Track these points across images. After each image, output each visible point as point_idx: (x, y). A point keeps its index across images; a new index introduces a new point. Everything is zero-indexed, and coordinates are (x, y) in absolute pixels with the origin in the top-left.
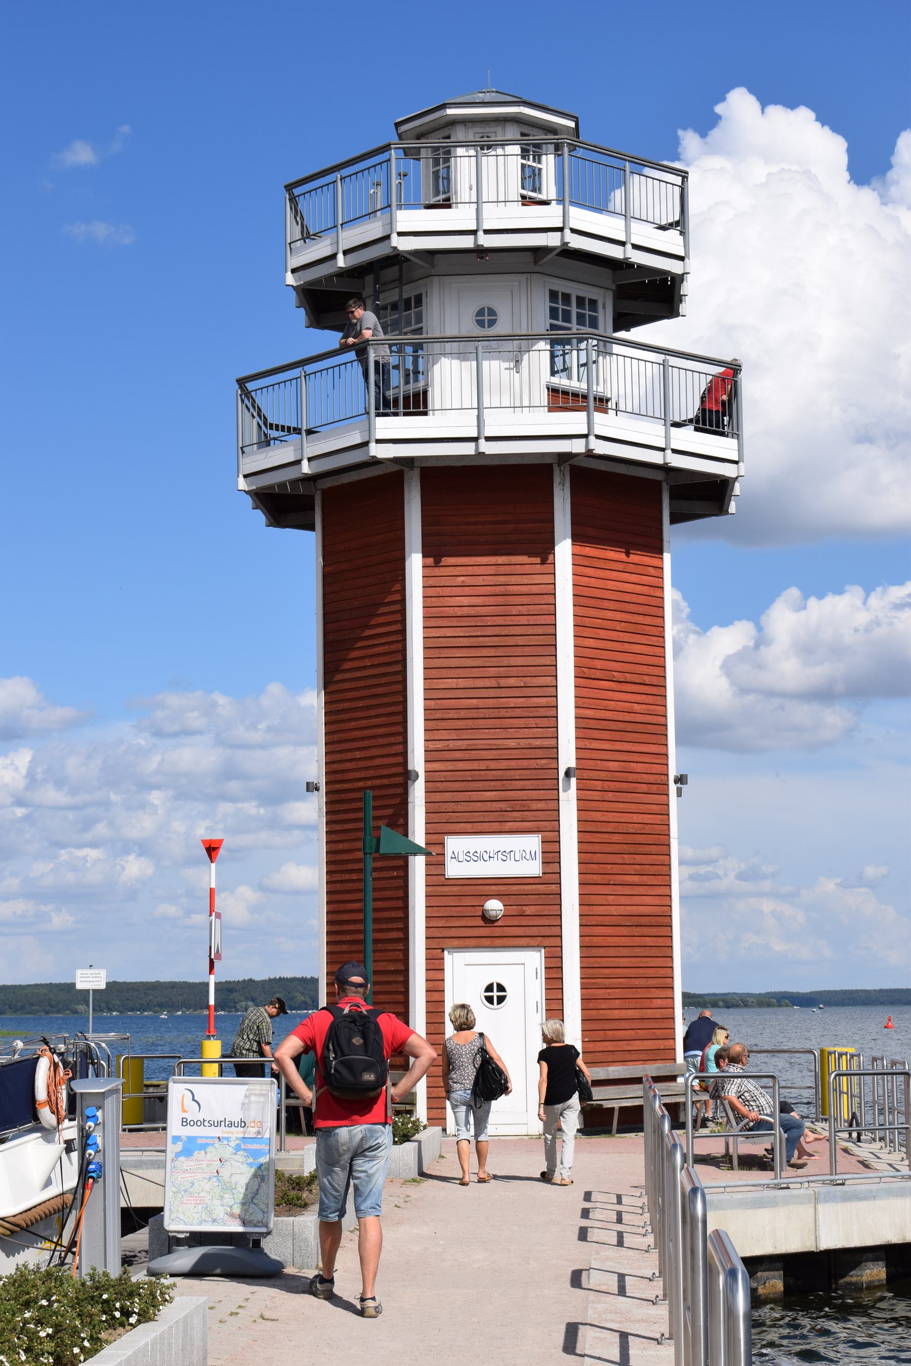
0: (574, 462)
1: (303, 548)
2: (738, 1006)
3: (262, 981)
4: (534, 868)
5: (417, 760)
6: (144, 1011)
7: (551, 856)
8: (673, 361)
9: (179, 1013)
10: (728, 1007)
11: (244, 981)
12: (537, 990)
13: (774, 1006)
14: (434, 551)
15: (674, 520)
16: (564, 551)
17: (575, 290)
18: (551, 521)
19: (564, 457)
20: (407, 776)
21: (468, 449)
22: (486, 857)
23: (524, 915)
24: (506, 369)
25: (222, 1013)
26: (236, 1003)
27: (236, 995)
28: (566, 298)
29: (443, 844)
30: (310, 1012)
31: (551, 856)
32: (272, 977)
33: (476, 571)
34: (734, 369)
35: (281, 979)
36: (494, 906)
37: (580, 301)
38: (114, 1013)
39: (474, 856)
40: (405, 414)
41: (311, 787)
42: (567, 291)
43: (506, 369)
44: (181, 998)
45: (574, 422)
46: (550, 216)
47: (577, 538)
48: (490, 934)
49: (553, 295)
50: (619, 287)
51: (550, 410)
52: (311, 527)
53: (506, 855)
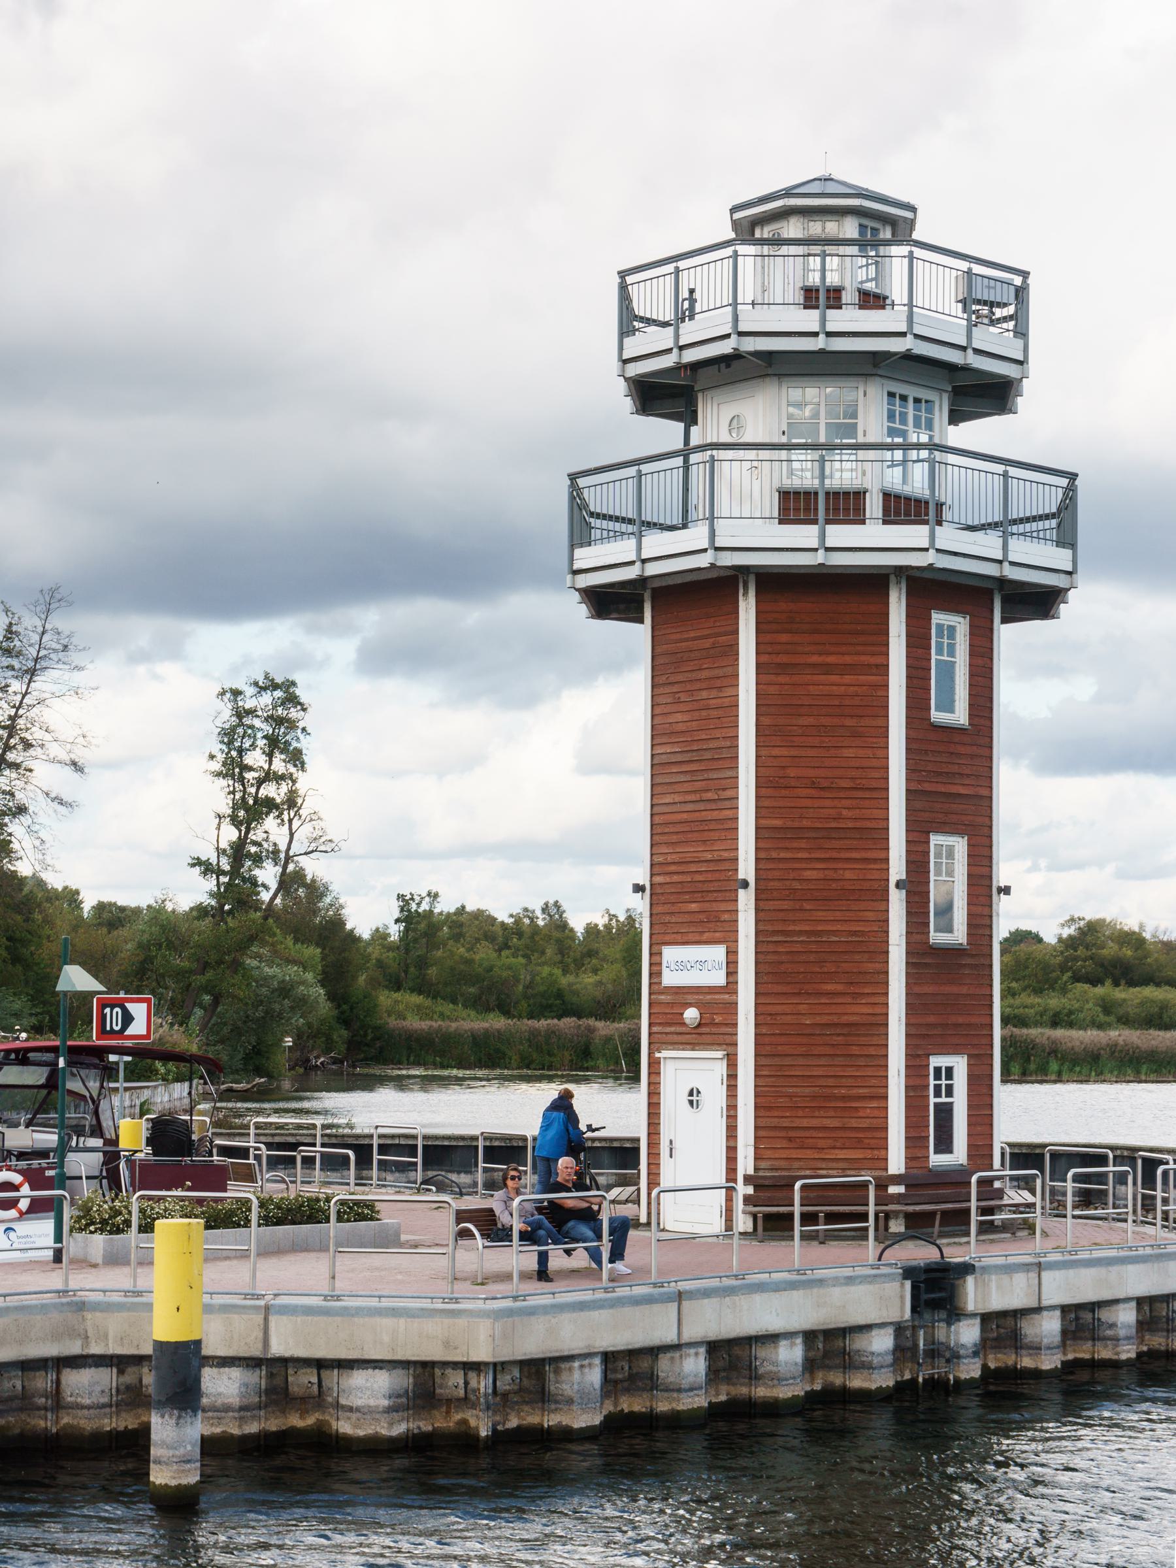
0: (910, 573)
1: (634, 638)
4: (718, 978)
8: (1013, 471)
15: (1004, 620)
17: (912, 392)
18: (886, 615)
19: (899, 570)
28: (904, 398)
37: (917, 401)
42: (904, 392)
45: (914, 535)
49: (891, 395)
50: (954, 387)
51: (885, 522)
52: (641, 621)
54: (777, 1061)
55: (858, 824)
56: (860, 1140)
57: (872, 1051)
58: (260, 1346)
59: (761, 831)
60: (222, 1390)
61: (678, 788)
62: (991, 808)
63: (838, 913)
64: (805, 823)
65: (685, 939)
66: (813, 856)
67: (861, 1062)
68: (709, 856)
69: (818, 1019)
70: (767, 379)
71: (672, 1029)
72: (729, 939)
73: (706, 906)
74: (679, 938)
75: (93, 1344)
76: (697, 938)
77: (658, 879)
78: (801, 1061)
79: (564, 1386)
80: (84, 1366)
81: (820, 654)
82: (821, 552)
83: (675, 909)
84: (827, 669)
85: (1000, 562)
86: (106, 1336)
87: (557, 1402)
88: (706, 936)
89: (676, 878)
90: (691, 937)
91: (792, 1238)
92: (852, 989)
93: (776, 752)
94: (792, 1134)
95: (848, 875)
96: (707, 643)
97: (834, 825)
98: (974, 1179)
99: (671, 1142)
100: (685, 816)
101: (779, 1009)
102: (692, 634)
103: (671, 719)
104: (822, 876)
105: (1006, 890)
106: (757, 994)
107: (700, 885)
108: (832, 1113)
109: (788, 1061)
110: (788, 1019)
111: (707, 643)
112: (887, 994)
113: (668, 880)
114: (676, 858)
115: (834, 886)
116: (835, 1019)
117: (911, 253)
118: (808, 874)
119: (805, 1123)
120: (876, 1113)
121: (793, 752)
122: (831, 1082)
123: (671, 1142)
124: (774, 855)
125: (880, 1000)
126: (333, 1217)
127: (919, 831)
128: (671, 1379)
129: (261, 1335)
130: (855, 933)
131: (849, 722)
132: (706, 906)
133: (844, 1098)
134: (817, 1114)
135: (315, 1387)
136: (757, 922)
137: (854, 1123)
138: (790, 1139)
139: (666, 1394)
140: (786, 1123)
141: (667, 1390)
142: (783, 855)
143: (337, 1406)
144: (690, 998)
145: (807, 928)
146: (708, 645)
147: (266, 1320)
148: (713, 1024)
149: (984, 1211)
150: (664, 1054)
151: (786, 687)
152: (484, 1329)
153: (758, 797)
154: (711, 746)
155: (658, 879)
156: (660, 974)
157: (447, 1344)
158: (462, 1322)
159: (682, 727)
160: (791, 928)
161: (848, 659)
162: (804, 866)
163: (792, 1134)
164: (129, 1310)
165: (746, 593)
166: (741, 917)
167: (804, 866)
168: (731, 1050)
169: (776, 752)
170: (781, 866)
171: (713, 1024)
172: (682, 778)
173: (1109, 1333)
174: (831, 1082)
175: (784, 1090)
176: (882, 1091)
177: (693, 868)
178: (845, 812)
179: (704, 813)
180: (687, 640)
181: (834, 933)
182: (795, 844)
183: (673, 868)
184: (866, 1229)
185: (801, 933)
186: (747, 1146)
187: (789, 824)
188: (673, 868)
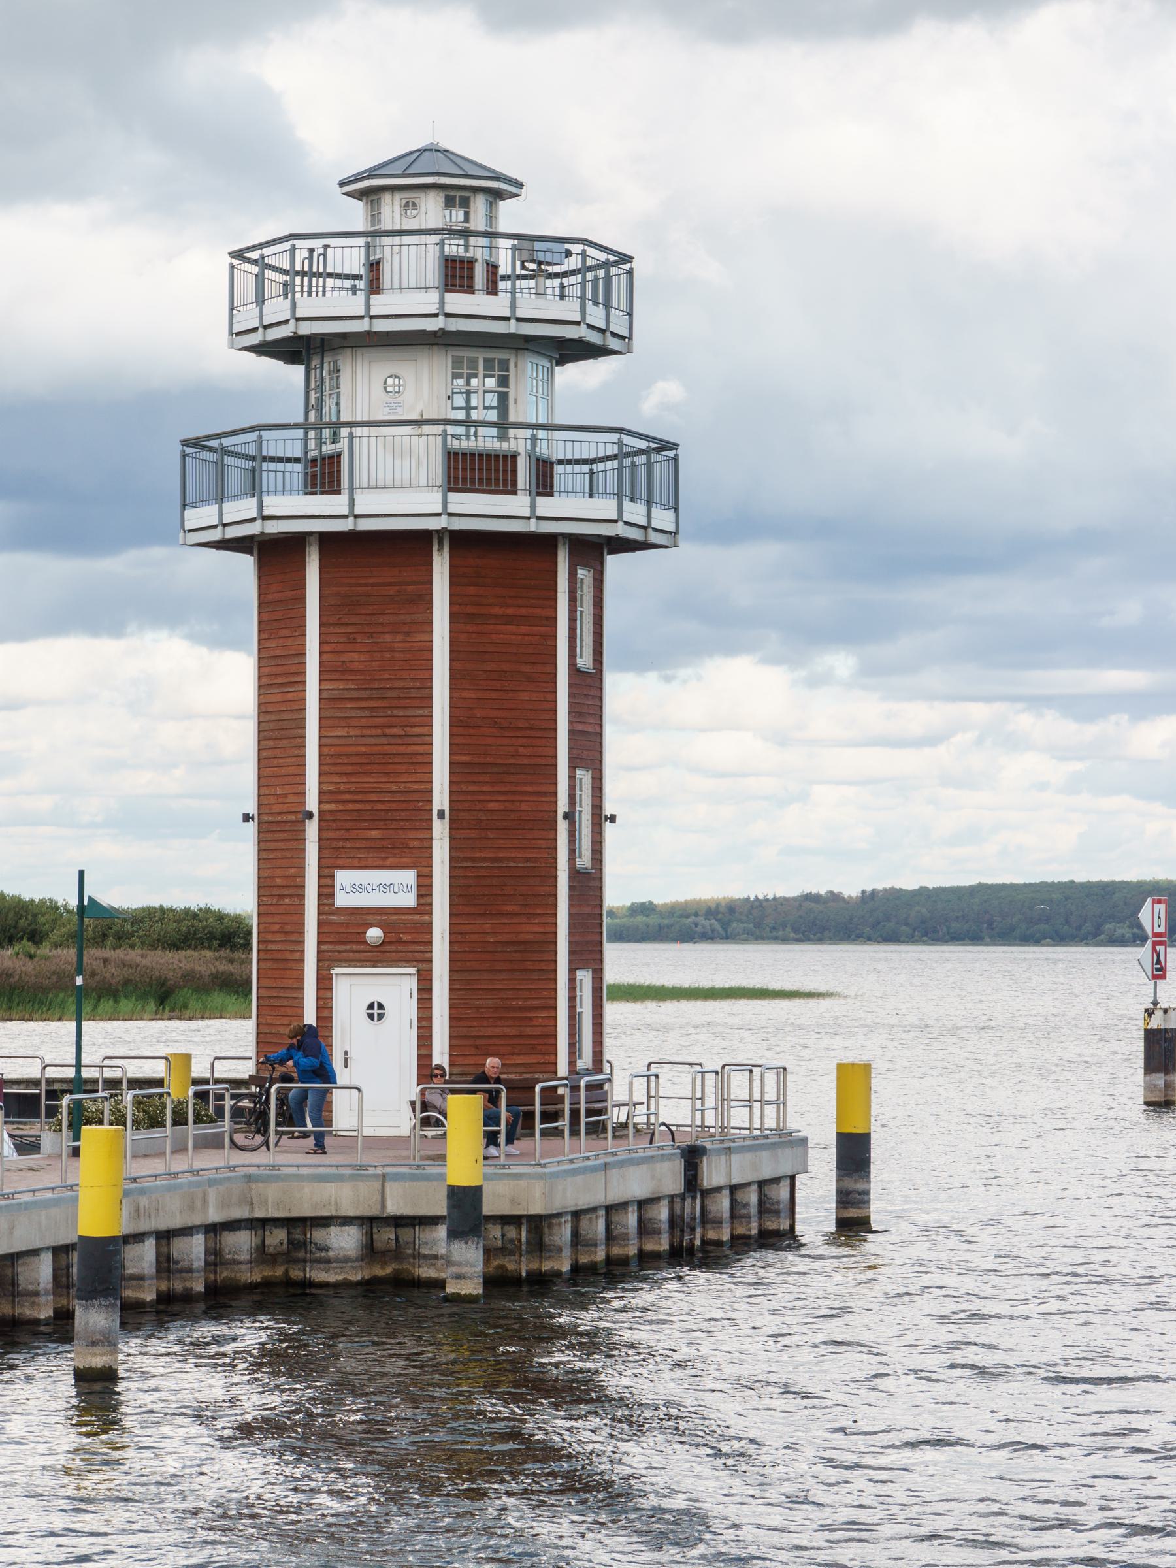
0: (256, 539)
4: (409, 900)
7: (424, 889)
12: (411, 1009)
22: (369, 889)
29: (332, 877)
31: (424, 889)
34: (186, 443)
40: (323, 493)
41: (247, 818)
48: (378, 956)
53: (386, 887)
54: (466, 976)
55: (532, 761)
56: (533, 1047)
57: (543, 966)
58: (379, 1207)
59: (455, 768)
60: (343, 1244)
61: (355, 722)
62: (601, 743)
63: (516, 842)
64: (489, 760)
65: (363, 863)
66: (496, 789)
67: (535, 976)
68: (394, 788)
69: (499, 938)
70: (435, 347)
71: (348, 947)
72: (422, 863)
73: (390, 834)
74: (356, 862)
75: (257, 1209)
76: (380, 862)
77: (327, 807)
78: (486, 976)
79: (556, 1238)
80: (239, 1229)
81: (501, 607)
82: (533, 521)
83: (353, 834)
84: (509, 620)
85: (645, 528)
86: (266, 1202)
87: (550, 1251)
88: (389, 861)
89: (350, 806)
90: (363, 863)
91: (533, 1135)
92: (528, 910)
93: (465, 694)
94: (479, 1042)
95: (524, 807)
96: (392, 591)
97: (512, 761)
98: (583, 1083)
99: (346, 1053)
100: (363, 749)
101: (468, 928)
102: (371, 581)
103: (345, 657)
104: (502, 807)
105: (612, 819)
106: (451, 915)
107: (383, 814)
108: (510, 1023)
109: (475, 976)
110: (475, 937)
111: (392, 591)
112: (556, 915)
113: (341, 807)
114: (352, 787)
115: (513, 817)
116: (514, 938)
117: (584, 251)
118: (491, 806)
119: (489, 1032)
120: (547, 1022)
121: (479, 695)
122: (510, 994)
123: (346, 1053)
124: (464, 788)
125: (551, 919)
126: (169, 1122)
127: (572, 768)
128: (590, 1236)
129: (379, 1198)
130: (528, 860)
131: (526, 668)
132: (390, 834)
133: (520, 1009)
134: (499, 1023)
135: (393, 1243)
136: (451, 848)
137: (529, 1031)
138: (477, 1047)
139: (586, 1249)
140: (474, 1032)
141: (586, 1245)
142: (471, 788)
143: (420, 1256)
144: (370, 919)
145: (490, 855)
146: (392, 592)
147: (383, 1186)
148: (400, 942)
149: (590, 1113)
150: (335, 971)
151: (474, 636)
152: (538, 1189)
153: (451, 735)
154: (396, 685)
155: (327, 807)
156: (332, 895)
157: (513, 1201)
158: (523, 1183)
159: (356, 665)
160: (478, 855)
161: (523, 611)
162: (488, 798)
163: (479, 1042)
164: (283, 1180)
165: (440, 549)
166: (436, 845)
167: (488, 798)
168: (424, 966)
169: (465, 694)
170: (469, 798)
171: (400, 942)
172: (359, 713)
173: (744, 1211)
174: (510, 994)
175: (472, 1002)
176: (551, 1002)
177: (374, 797)
178: (521, 750)
179: (386, 748)
180: (366, 585)
181: (513, 859)
182: (481, 778)
183: (347, 797)
184: (499, 1132)
185: (485, 859)
186: (442, 1053)
187: (476, 760)
188: (347, 797)
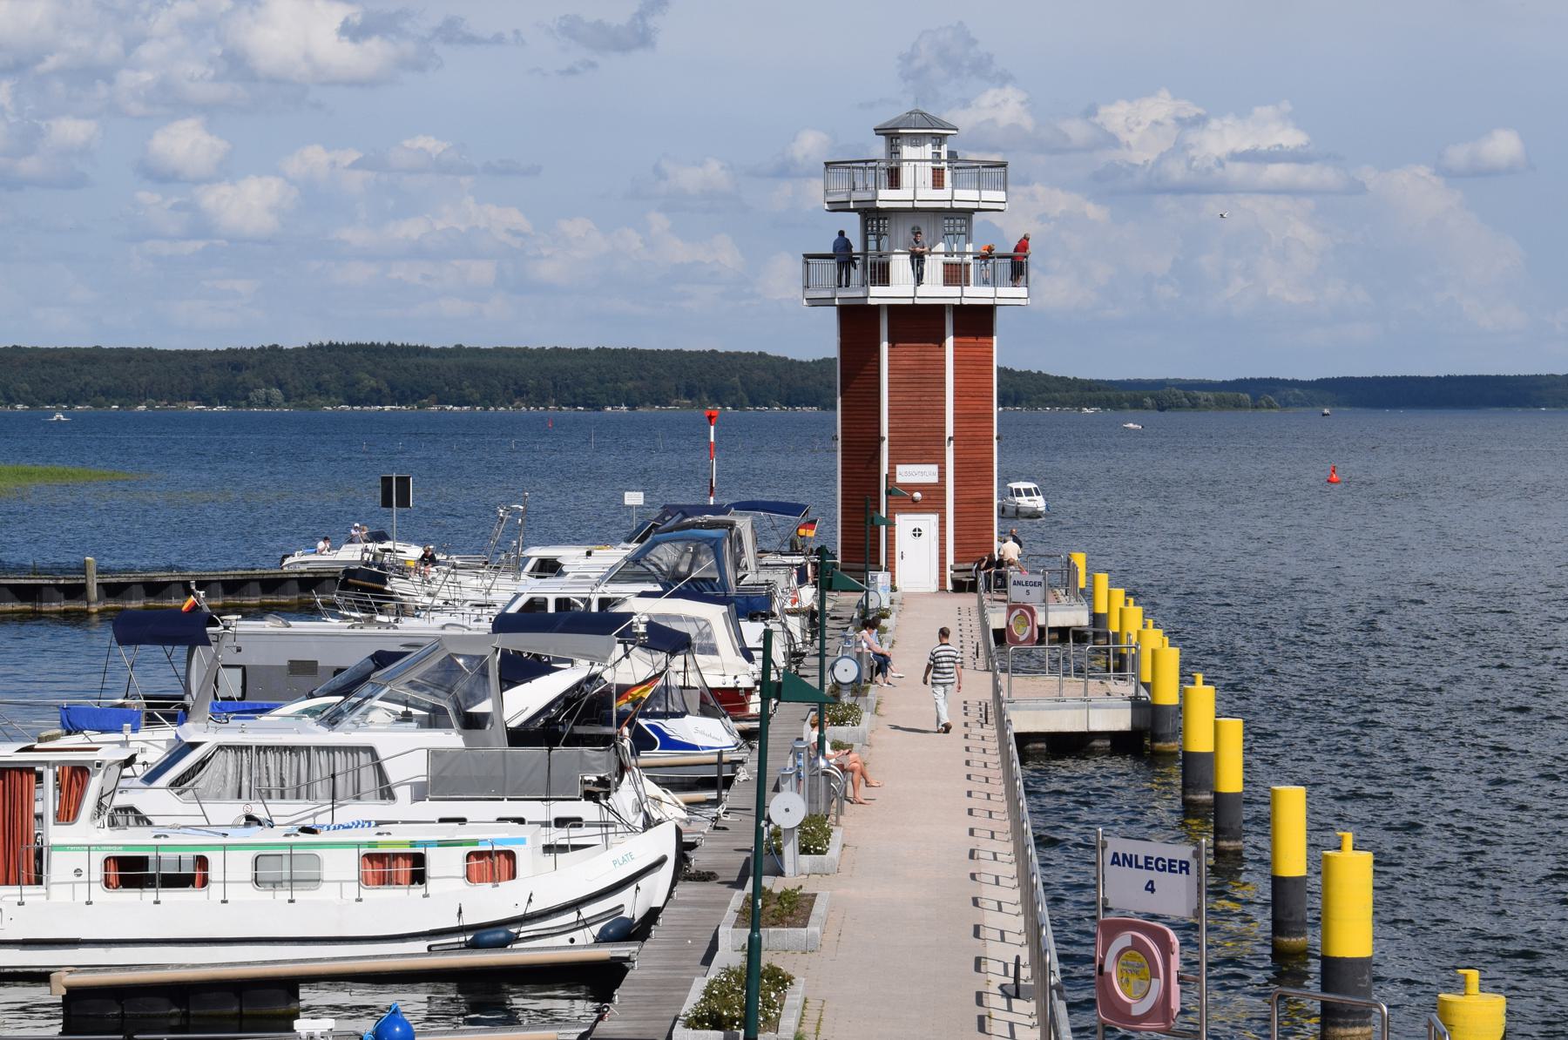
2: (1178, 406)
3: (297, 350)
4: (935, 479)
5: (885, 432)
6: (76, 402)
7: (942, 474)
9: (142, 408)
10: (1162, 409)
11: (262, 349)
13: (1246, 407)
14: (893, 341)
16: (950, 341)
20: (880, 439)
21: (910, 302)
23: (931, 499)
24: (1018, 958)
25: (223, 408)
26: (248, 390)
27: (247, 375)
30: (387, 408)
31: (942, 474)
32: (315, 342)
33: (911, 350)
35: (332, 347)
36: (917, 495)
38: (19, 407)
39: (908, 474)
43: (1018, 958)
44: (144, 380)
46: (944, 194)
47: (955, 335)
48: (915, 507)
53: (923, 473)
